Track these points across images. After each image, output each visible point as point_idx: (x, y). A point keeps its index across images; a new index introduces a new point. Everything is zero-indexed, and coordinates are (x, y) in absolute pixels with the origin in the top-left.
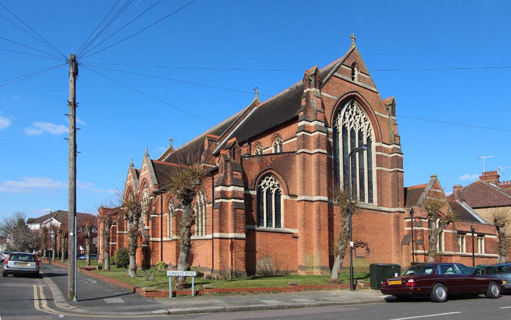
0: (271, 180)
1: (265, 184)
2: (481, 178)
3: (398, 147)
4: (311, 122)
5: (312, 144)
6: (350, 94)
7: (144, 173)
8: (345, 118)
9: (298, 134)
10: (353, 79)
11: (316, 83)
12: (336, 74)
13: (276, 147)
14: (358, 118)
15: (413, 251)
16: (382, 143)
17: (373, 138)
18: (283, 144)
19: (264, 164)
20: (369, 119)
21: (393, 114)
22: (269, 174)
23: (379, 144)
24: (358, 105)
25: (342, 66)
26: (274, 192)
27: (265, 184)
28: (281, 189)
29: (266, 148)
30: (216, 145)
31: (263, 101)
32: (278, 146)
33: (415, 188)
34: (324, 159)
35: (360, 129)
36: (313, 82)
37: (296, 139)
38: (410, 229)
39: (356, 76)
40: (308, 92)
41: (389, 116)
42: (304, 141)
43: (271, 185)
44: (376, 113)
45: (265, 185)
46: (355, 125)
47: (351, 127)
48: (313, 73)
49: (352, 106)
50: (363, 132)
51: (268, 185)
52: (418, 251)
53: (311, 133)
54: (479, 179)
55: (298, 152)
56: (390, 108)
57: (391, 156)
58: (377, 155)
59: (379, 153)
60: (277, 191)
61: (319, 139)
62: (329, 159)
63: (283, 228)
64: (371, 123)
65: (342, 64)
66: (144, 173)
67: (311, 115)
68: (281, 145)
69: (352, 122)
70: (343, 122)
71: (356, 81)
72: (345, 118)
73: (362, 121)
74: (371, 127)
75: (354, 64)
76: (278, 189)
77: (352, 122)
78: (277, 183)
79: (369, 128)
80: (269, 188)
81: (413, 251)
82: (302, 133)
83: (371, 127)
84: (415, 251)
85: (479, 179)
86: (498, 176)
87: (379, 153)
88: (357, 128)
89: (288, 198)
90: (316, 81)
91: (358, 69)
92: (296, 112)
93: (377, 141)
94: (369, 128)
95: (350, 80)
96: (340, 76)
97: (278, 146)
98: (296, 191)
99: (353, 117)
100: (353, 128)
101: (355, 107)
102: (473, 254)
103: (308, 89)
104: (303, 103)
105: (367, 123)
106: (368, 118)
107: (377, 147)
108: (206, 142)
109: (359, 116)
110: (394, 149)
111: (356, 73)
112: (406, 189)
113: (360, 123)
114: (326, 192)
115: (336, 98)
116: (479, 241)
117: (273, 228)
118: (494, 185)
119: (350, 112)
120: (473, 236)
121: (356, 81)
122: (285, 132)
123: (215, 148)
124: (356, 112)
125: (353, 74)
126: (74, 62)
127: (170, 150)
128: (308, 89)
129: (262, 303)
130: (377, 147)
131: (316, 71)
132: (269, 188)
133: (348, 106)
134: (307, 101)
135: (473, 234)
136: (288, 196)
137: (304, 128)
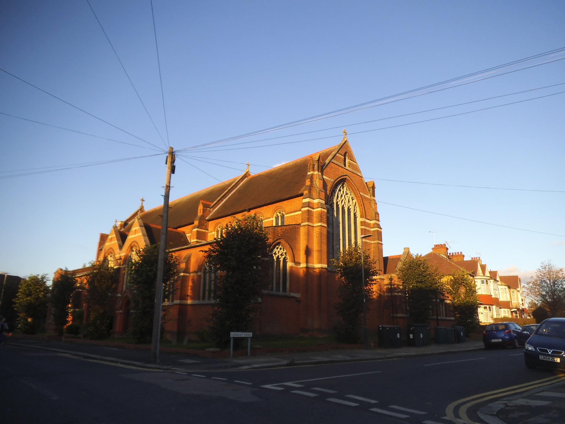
0: (281, 249)
1: (276, 252)
2: (433, 249)
3: (377, 222)
4: (314, 199)
5: (315, 219)
6: (343, 177)
7: (134, 236)
8: (338, 197)
9: (303, 209)
10: (345, 166)
11: (318, 167)
12: (333, 161)
13: (277, 218)
14: (347, 197)
15: (393, 315)
16: (366, 218)
17: (358, 215)
18: (285, 216)
19: (276, 234)
20: (356, 199)
21: (374, 195)
22: (279, 244)
23: (363, 220)
24: (348, 187)
25: (338, 154)
26: (282, 259)
27: (276, 252)
28: (288, 256)
29: (267, 218)
30: (210, 212)
31: (255, 171)
32: (280, 218)
33: (395, 258)
34: (325, 232)
35: (349, 206)
36: (316, 167)
37: (300, 212)
38: (390, 294)
39: (347, 164)
40: (312, 175)
41: (370, 196)
42: (309, 216)
43: (280, 253)
44: (361, 194)
45: (275, 254)
46: (345, 203)
47: (343, 204)
48: (372, 186)
49: (343, 187)
50: (350, 209)
51: (278, 253)
52: (398, 315)
53: (314, 209)
54: (431, 251)
55: (302, 224)
56: (371, 190)
57: (372, 230)
58: (362, 229)
59: (363, 227)
60: (285, 259)
61: (321, 214)
62: (328, 232)
63: (287, 293)
64: (357, 203)
65: (338, 152)
66: (134, 236)
67: (314, 194)
68: (283, 217)
69: (343, 200)
70: (337, 200)
71: (347, 167)
72: (338, 197)
73: (351, 199)
74: (357, 205)
75: (346, 153)
76: (285, 257)
77: (343, 200)
78: (285, 251)
79: (355, 205)
80: (279, 256)
81: (393, 315)
82: (307, 208)
83: (357, 205)
84: (394, 315)
85: (431, 251)
86: (447, 249)
87: (363, 227)
88: (347, 205)
89: (293, 265)
90: (318, 165)
91: (348, 157)
92: (300, 189)
93: (362, 217)
94: (355, 205)
95: (343, 166)
96: (335, 162)
97: (280, 218)
98: (300, 259)
99: (343, 196)
100: (343, 205)
101: (345, 188)
102: (438, 317)
103: (312, 172)
104: (308, 183)
105: (354, 201)
106: (355, 197)
107: (361, 222)
108: (201, 207)
109: (348, 196)
110: (374, 224)
111: (347, 160)
112: (386, 259)
113: (349, 201)
114: (326, 260)
115: (333, 180)
116: (441, 305)
117: (281, 293)
118: (444, 256)
119: (342, 191)
120: (436, 301)
121: (347, 167)
122: (287, 205)
123: (209, 214)
124: (346, 192)
125: (345, 161)
126: (172, 155)
127: (142, 209)
128: (312, 172)
129: (313, 359)
130: (361, 222)
131: (373, 185)
132: (279, 256)
133: (340, 187)
134: (312, 181)
135: (436, 300)
136: (293, 263)
137: (309, 205)
